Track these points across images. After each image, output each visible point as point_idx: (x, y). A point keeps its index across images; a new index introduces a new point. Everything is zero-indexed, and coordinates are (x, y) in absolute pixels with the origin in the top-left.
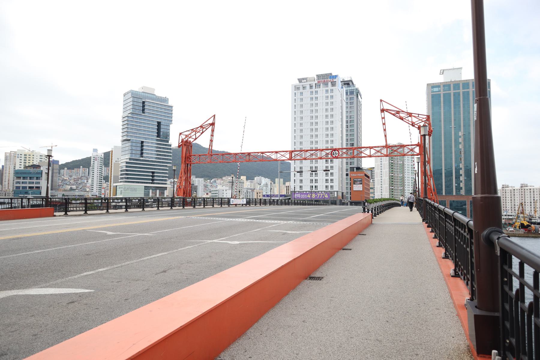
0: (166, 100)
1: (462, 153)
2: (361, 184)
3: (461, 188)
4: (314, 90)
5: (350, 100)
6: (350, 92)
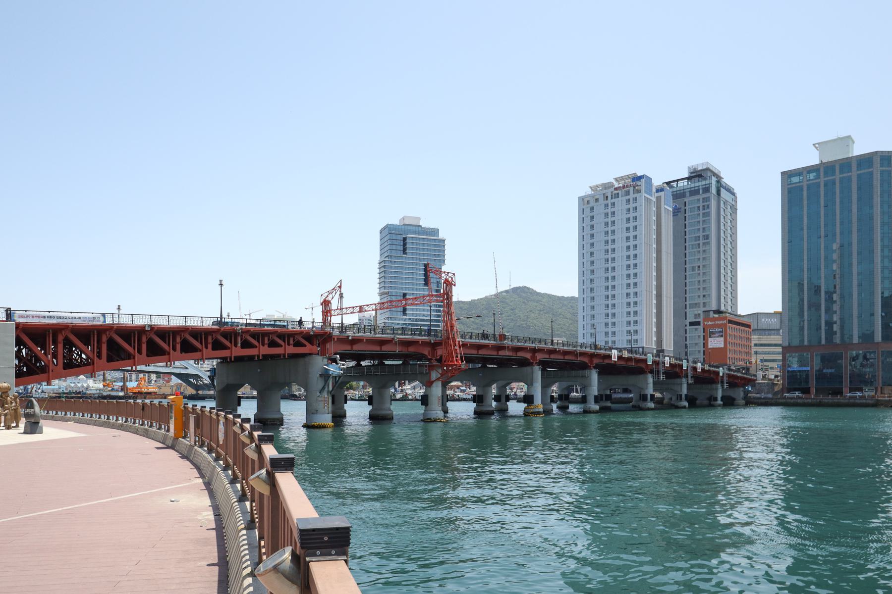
0: (435, 232)
1: (837, 276)
2: (722, 336)
3: (835, 333)
4: (610, 201)
5: (703, 202)
6: (702, 189)
